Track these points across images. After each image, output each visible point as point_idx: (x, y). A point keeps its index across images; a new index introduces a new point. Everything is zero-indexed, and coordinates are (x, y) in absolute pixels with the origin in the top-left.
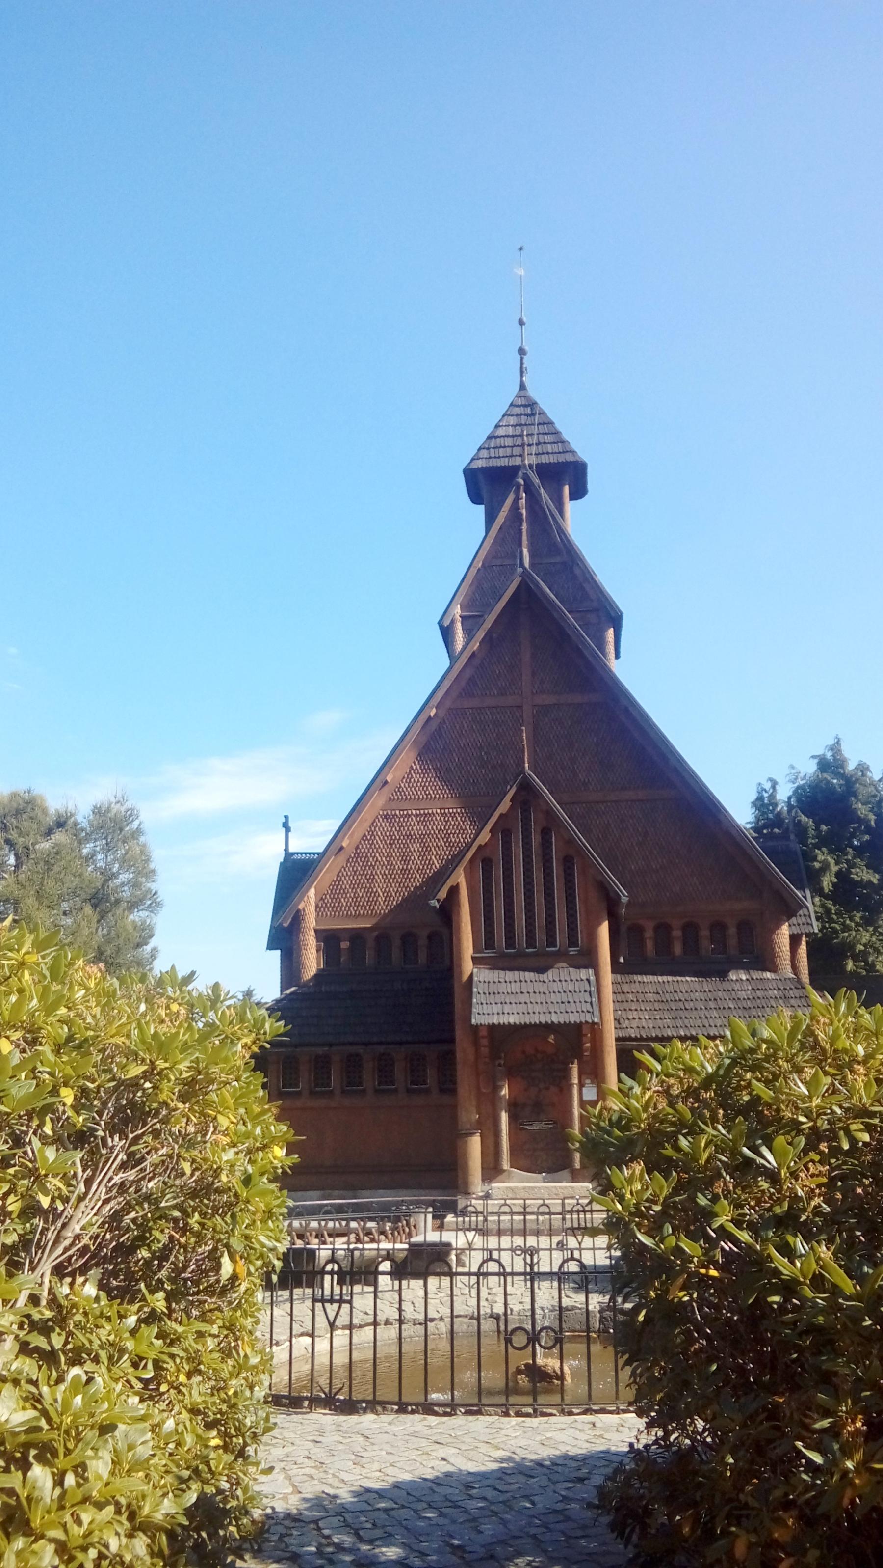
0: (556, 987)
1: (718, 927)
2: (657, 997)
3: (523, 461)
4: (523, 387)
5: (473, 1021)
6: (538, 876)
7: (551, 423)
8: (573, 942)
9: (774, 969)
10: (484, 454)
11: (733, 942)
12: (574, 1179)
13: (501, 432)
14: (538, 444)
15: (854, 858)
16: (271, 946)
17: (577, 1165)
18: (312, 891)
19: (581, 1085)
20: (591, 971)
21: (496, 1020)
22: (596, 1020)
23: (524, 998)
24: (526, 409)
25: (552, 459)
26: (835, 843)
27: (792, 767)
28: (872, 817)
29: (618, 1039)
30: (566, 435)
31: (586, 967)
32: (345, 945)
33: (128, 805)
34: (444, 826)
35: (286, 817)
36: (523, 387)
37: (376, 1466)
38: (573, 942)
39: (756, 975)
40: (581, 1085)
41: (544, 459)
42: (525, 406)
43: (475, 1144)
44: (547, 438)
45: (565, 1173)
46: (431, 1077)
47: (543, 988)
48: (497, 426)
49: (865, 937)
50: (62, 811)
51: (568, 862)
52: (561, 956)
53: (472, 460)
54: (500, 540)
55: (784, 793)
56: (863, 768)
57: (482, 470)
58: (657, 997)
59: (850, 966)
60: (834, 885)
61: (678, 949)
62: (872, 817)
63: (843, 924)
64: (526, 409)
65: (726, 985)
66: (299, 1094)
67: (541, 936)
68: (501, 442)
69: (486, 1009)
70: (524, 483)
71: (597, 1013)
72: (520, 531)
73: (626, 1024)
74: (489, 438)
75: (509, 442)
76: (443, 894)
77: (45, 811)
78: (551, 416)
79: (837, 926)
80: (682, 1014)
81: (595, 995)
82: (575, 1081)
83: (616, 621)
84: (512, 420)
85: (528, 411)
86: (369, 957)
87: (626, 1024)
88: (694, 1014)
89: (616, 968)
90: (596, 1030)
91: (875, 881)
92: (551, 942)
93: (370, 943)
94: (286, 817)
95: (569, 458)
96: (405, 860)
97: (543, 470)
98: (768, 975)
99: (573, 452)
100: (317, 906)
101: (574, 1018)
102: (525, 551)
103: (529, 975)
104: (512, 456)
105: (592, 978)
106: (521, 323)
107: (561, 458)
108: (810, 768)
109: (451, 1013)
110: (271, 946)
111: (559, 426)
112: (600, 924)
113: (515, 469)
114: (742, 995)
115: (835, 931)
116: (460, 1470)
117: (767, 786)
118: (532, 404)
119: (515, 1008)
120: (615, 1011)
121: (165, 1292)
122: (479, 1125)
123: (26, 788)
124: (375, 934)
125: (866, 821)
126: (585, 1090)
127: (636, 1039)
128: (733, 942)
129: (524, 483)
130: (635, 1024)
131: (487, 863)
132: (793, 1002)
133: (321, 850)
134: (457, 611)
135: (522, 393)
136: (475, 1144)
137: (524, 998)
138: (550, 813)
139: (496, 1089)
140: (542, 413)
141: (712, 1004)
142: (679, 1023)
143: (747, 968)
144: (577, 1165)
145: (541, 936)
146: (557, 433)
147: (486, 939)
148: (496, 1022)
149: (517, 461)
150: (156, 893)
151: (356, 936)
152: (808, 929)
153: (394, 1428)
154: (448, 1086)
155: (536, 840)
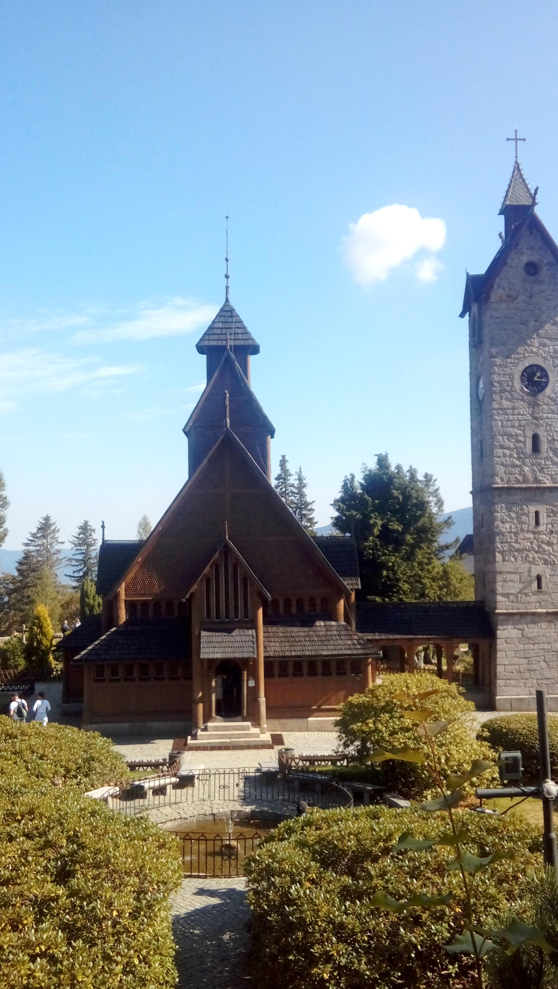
0: (238, 638)
1: (312, 600)
2: (283, 635)
3: (227, 343)
4: (227, 300)
5: (201, 657)
6: (231, 586)
7: (241, 322)
8: (246, 616)
9: (336, 620)
11: (318, 607)
12: (244, 720)
13: (216, 325)
14: (235, 334)
15: (391, 517)
17: (245, 715)
18: (123, 585)
19: (248, 680)
20: (254, 631)
21: (211, 656)
22: (255, 656)
23: (224, 645)
26: (381, 510)
27: (364, 464)
28: (401, 497)
29: (264, 657)
30: (250, 329)
31: (252, 629)
35: (103, 522)
36: (227, 300)
37: (189, 900)
38: (246, 616)
39: (328, 623)
40: (248, 680)
41: (238, 343)
42: (228, 311)
43: (201, 706)
44: (239, 331)
45: (239, 718)
46: (180, 672)
47: (232, 639)
49: (393, 559)
54: (215, 386)
55: (359, 479)
58: (283, 635)
59: (385, 573)
60: (380, 531)
61: (294, 610)
62: (401, 497)
63: (383, 552)
65: (314, 628)
66: (119, 680)
67: (232, 613)
68: (215, 331)
69: (207, 650)
70: (227, 352)
71: (256, 653)
72: (226, 411)
73: (269, 649)
76: (188, 596)
78: (242, 317)
79: (380, 553)
80: (294, 644)
81: (255, 643)
82: (246, 678)
83: (272, 432)
86: (151, 613)
87: (269, 649)
88: (299, 644)
89: (265, 623)
90: (255, 661)
91: (400, 529)
92: (237, 616)
93: (151, 607)
94: (103, 522)
95: (250, 342)
98: (333, 623)
99: (252, 339)
100: (125, 589)
101: (245, 655)
102: (228, 420)
105: (254, 634)
107: (246, 343)
108: (373, 465)
109: (191, 649)
111: (246, 323)
112: (259, 609)
113: (224, 348)
114: (321, 633)
115: (379, 555)
117: (349, 477)
118: (232, 310)
119: (220, 650)
120: (264, 642)
122: (202, 700)
124: (153, 602)
125: (397, 498)
126: (249, 682)
127: (273, 657)
128: (318, 607)
129: (227, 352)
130: (273, 649)
131: (208, 580)
132: (343, 637)
136: (201, 706)
137: (224, 645)
138: (237, 559)
139: (210, 682)
140: (237, 316)
141: (307, 639)
142: (292, 649)
143: (324, 620)
144: (245, 715)
145: (232, 613)
146: (244, 328)
148: (211, 657)
149: (224, 343)
150: (5, 498)
151: (145, 604)
152: (356, 587)
153: (190, 884)
154: (188, 677)
155: (230, 569)
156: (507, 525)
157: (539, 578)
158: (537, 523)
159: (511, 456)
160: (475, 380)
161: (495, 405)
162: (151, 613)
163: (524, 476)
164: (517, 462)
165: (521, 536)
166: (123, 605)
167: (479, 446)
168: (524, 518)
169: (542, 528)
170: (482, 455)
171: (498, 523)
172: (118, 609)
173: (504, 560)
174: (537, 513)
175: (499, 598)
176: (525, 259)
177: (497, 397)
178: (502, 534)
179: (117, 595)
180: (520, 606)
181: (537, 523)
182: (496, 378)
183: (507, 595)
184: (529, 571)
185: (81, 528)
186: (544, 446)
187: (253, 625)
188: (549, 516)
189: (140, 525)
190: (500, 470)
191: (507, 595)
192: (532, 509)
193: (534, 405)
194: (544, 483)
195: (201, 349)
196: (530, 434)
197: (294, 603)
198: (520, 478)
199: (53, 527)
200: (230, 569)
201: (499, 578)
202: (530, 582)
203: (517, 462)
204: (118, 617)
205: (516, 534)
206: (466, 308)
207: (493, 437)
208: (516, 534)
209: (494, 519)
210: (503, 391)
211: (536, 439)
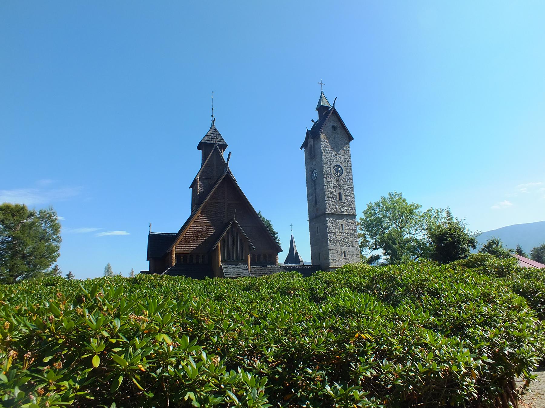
0: (241, 269)
10: (205, 139)
13: (209, 134)
16: (199, 148)
24: (214, 130)
25: (221, 143)
32: (182, 257)
33: (53, 211)
34: (207, 229)
50: (32, 211)
51: (241, 240)
52: (240, 262)
64: (214, 130)
70: (212, 149)
75: (211, 137)
76: (215, 247)
77: (27, 210)
84: (211, 132)
86: (188, 261)
92: (233, 258)
96: (197, 237)
97: (219, 145)
103: (234, 266)
110: (199, 148)
113: (214, 144)
121: (18, 326)
123: (22, 204)
129: (212, 149)
133: (175, 231)
134: (198, 177)
147: (223, 258)
151: (185, 255)
155: (234, 235)
156: (332, 230)
157: (344, 252)
158: (342, 229)
161: (325, 179)
162: (188, 261)
163: (337, 209)
164: (334, 203)
165: (337, 234)
166: (174, 256)
169: (344, 231)
170: (316, 203)
172: (171, 258)
174: (342, 225)
175: (331, 261)
176: (332, 124)
177: (325, 176)
178: (330, 233)
179: (172, 251)
180: (338, 264)
181: (342, 229)
182: (324, 168)
183: (333, 260)
185: (67, 275)
186: (343, 198)
187: (246, 262)
189: (106, 269)
190: (328, 206)
191: (333, 260)
192: (340, 222)
193: (338, 180)
194: (121, 339)
195: (200, 146)
197: (256, 257)
199: (58, 271)
200: (234, 235)
201: (330, 252)
202: (341, 254)
203: (334, 203)
204: (172, 262)
205: (335, 233)
206: (305, 145)
207: (324, 193)
208: (335, 233)
209: (327, 227)
210: (327, 174)
211: (340, 194)
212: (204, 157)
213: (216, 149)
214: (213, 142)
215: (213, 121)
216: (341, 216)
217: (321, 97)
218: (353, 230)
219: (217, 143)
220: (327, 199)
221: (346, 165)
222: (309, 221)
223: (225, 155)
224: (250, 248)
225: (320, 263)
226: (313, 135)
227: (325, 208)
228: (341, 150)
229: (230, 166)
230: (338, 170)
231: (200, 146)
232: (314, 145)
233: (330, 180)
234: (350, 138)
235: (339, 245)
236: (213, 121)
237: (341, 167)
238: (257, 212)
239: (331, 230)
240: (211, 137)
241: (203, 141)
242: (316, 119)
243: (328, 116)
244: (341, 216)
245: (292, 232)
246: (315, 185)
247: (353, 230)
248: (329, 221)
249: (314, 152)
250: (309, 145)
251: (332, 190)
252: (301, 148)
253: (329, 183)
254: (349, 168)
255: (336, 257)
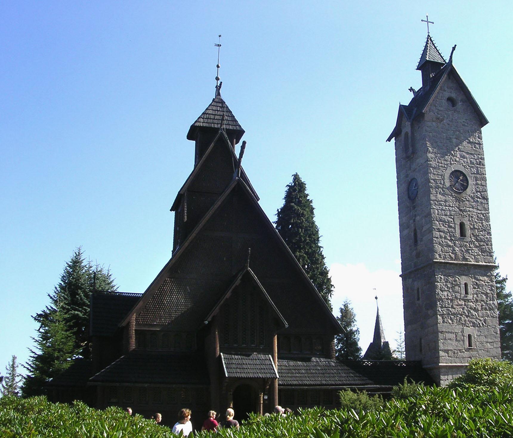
10: (202, 120)
13: (210, 112)
16: (190, 137)
24: (218, 102)
35: (455, 45)
36: (218, 94)
42: (220, 103)
48: (207, 109)
53: (196, 122)
56: (307, 195)
57: (200, 127)
64: (218, 102)
74: (203, 113)
85: (220, 105)
94: (455, 45)
97: (228, 131)
104: (214, 119)
106: (218, 66)
110: (190, 137)
113: (218, 129)
116: (109, 276)
118: (223, 102)
135: (218, 97)
156: (445, 293)
158: (467, 293)
159: (445, 238)
160: (405, 186)
161: (433, 198)
163: (456, 254)
167: (413, 234)
168: (457, 287)
169: (470, 297)
171: (438, 291)
173: (444, 322)
174: (466, 285)
176: (447, 95)
181: (467, 293)
183: (447, 351)
184: (462, 331)
186: (468, 232)
188: (475, 288)
190: (438, 248)
191: (447, 351)
192: (463, 280)
193: (458, 200)
195: (194, 133)
196: (458, 222)
198: (453, 256)
201: (441, 336)
207: (431, 222)
208: (452, 300)
209: (435, 287)
211: (462, 225)
212: (199, 153)
213: (222, 139)
214: (216, 126)
215: (218, 88)
216: (466, 269)
217: (426, 47)
218: (486, 294)
219: (224, 126)
220: (436, 234)
221: (474, 170)
222: (404, 276)
223: (237, 149)
224: (278, 323)
225: (420, 366)
226: (411, 116)
227: (432, 251)
228: (465, 143)
229: (244, 164)
230: (460, 180)
231: (194, 133)
232: (412, 133)
233: (443, 198)
234: (482, 121)
235: (459, 321)
236: (218, 88)
237: (464, 175)
238: (284, 200)
239: (444, 295)
240: (212, 117)
241: (197, 124)
242: (418, 85)
243: (438, 74)
244: (466, 269)
245: (366, 286)
246: (414, 207)
247: (486, 294)
248: (441, 281)
249: (413, 146)
250: (403, 133)
251: (447, 218)
252: (389, 140)
253: (441, 205)
254: (481, 177)
255: (452, 345)
